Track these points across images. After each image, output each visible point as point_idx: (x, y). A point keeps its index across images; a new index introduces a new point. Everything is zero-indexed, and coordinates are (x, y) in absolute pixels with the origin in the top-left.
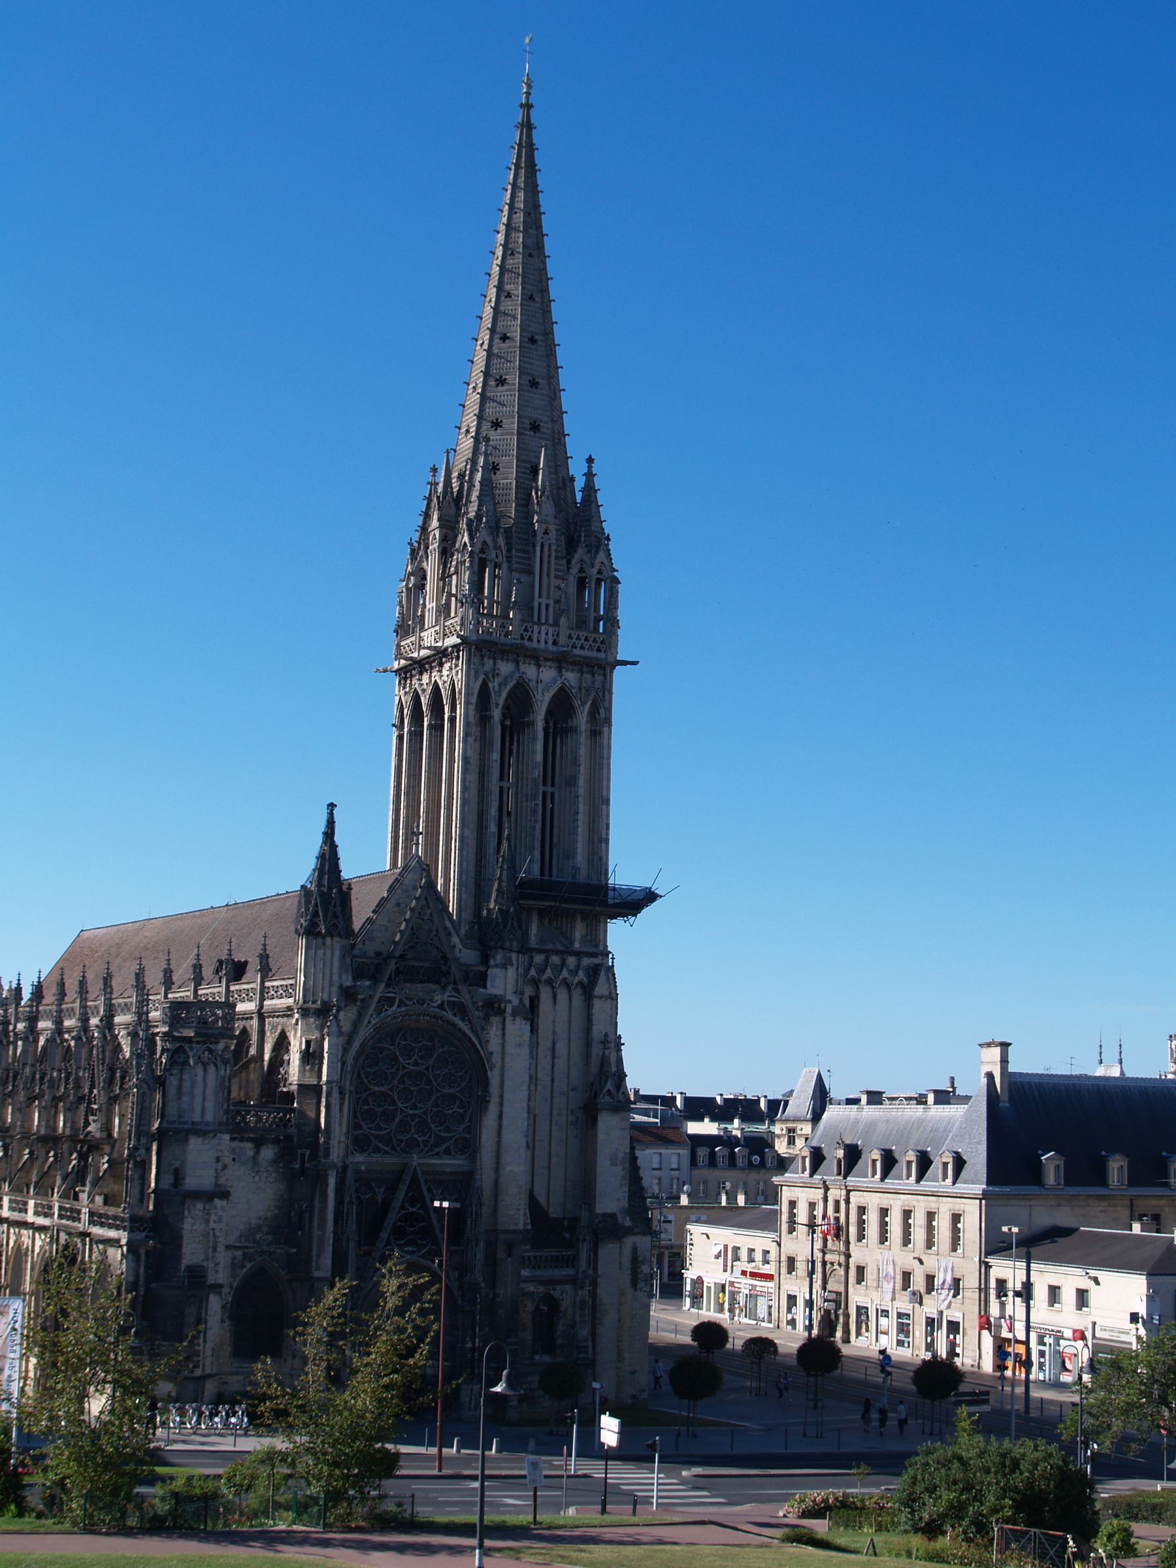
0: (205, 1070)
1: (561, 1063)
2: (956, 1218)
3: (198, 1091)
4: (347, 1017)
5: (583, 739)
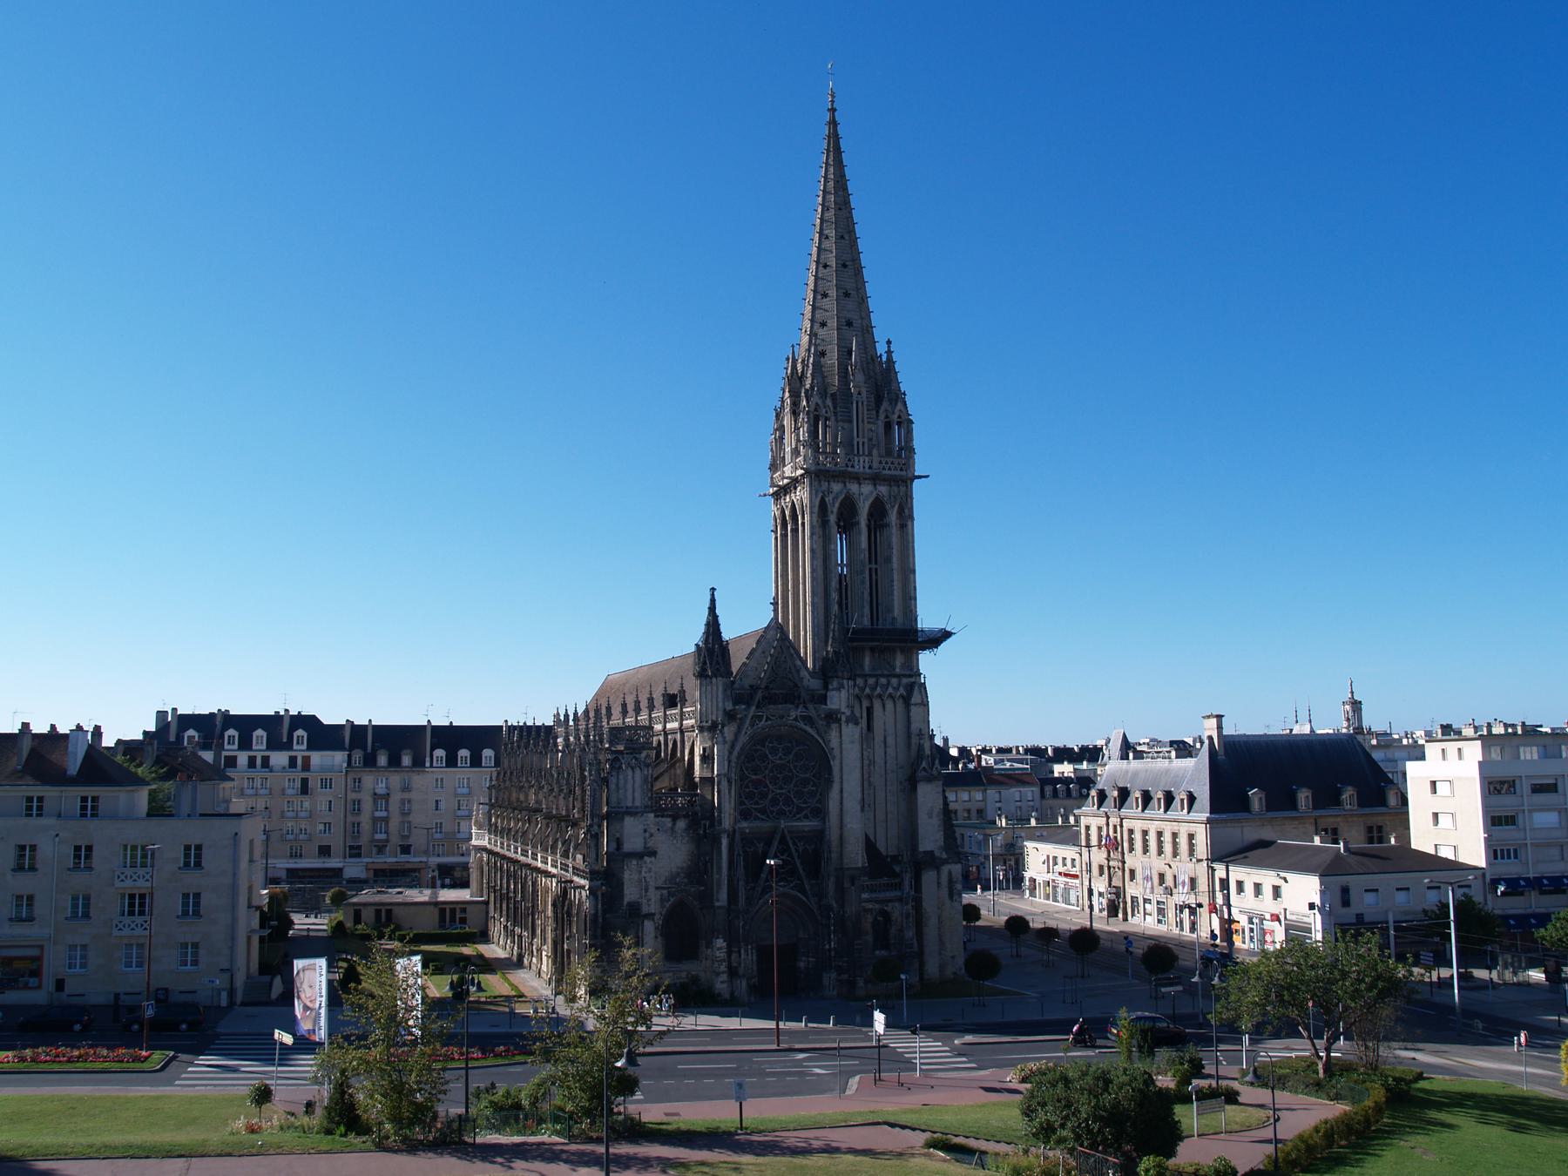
1: (890, 751)
2: (1191, 837)
3: (629, 786)
4: (729, 731)
5: (894, 530)
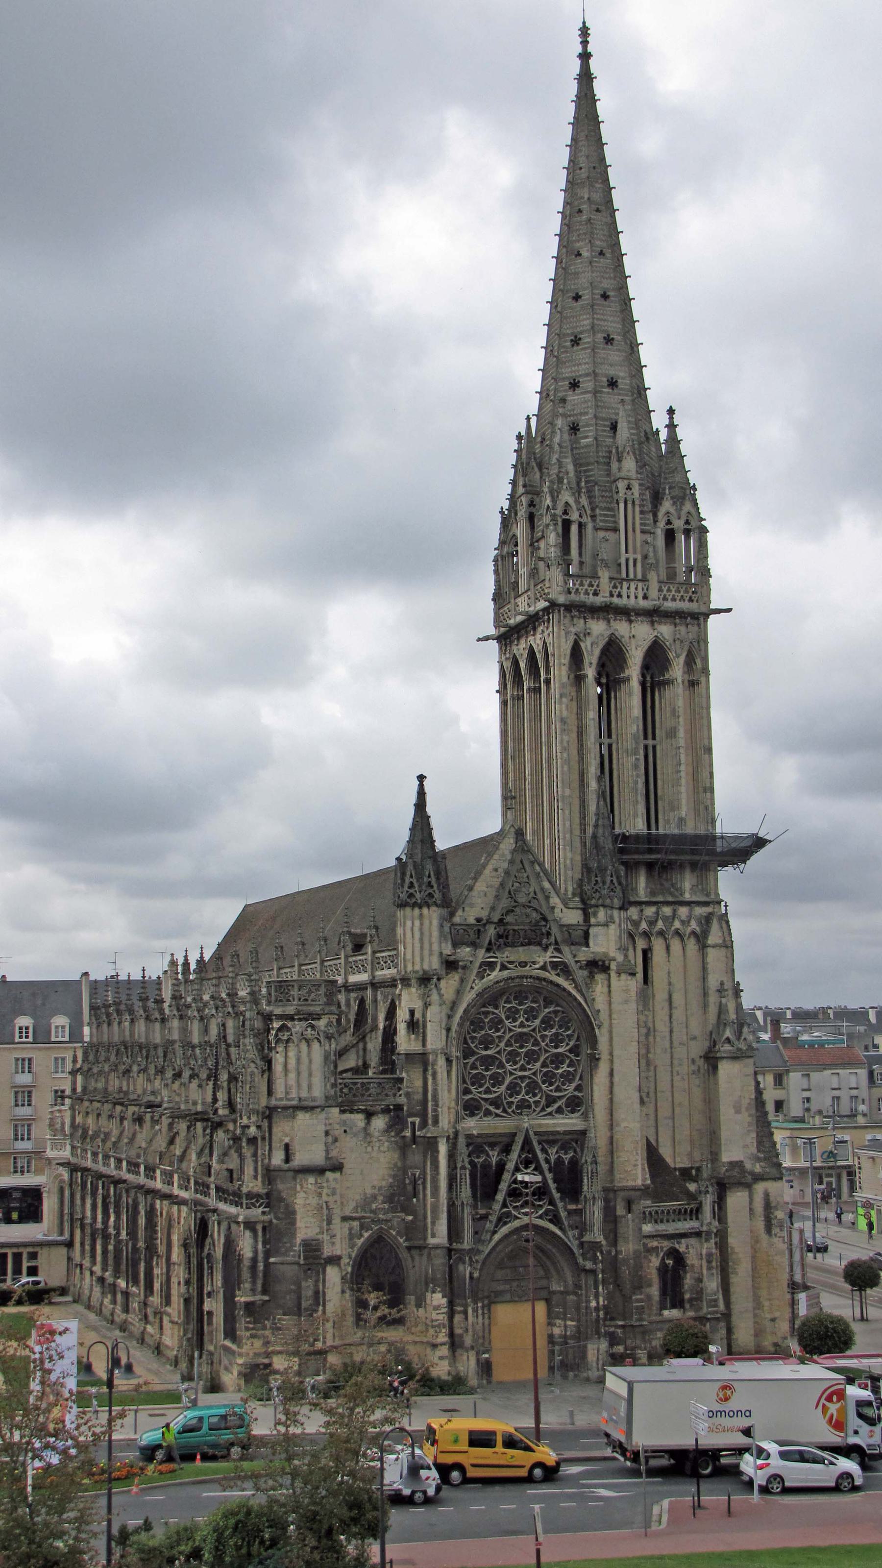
0: (309, 1046)
